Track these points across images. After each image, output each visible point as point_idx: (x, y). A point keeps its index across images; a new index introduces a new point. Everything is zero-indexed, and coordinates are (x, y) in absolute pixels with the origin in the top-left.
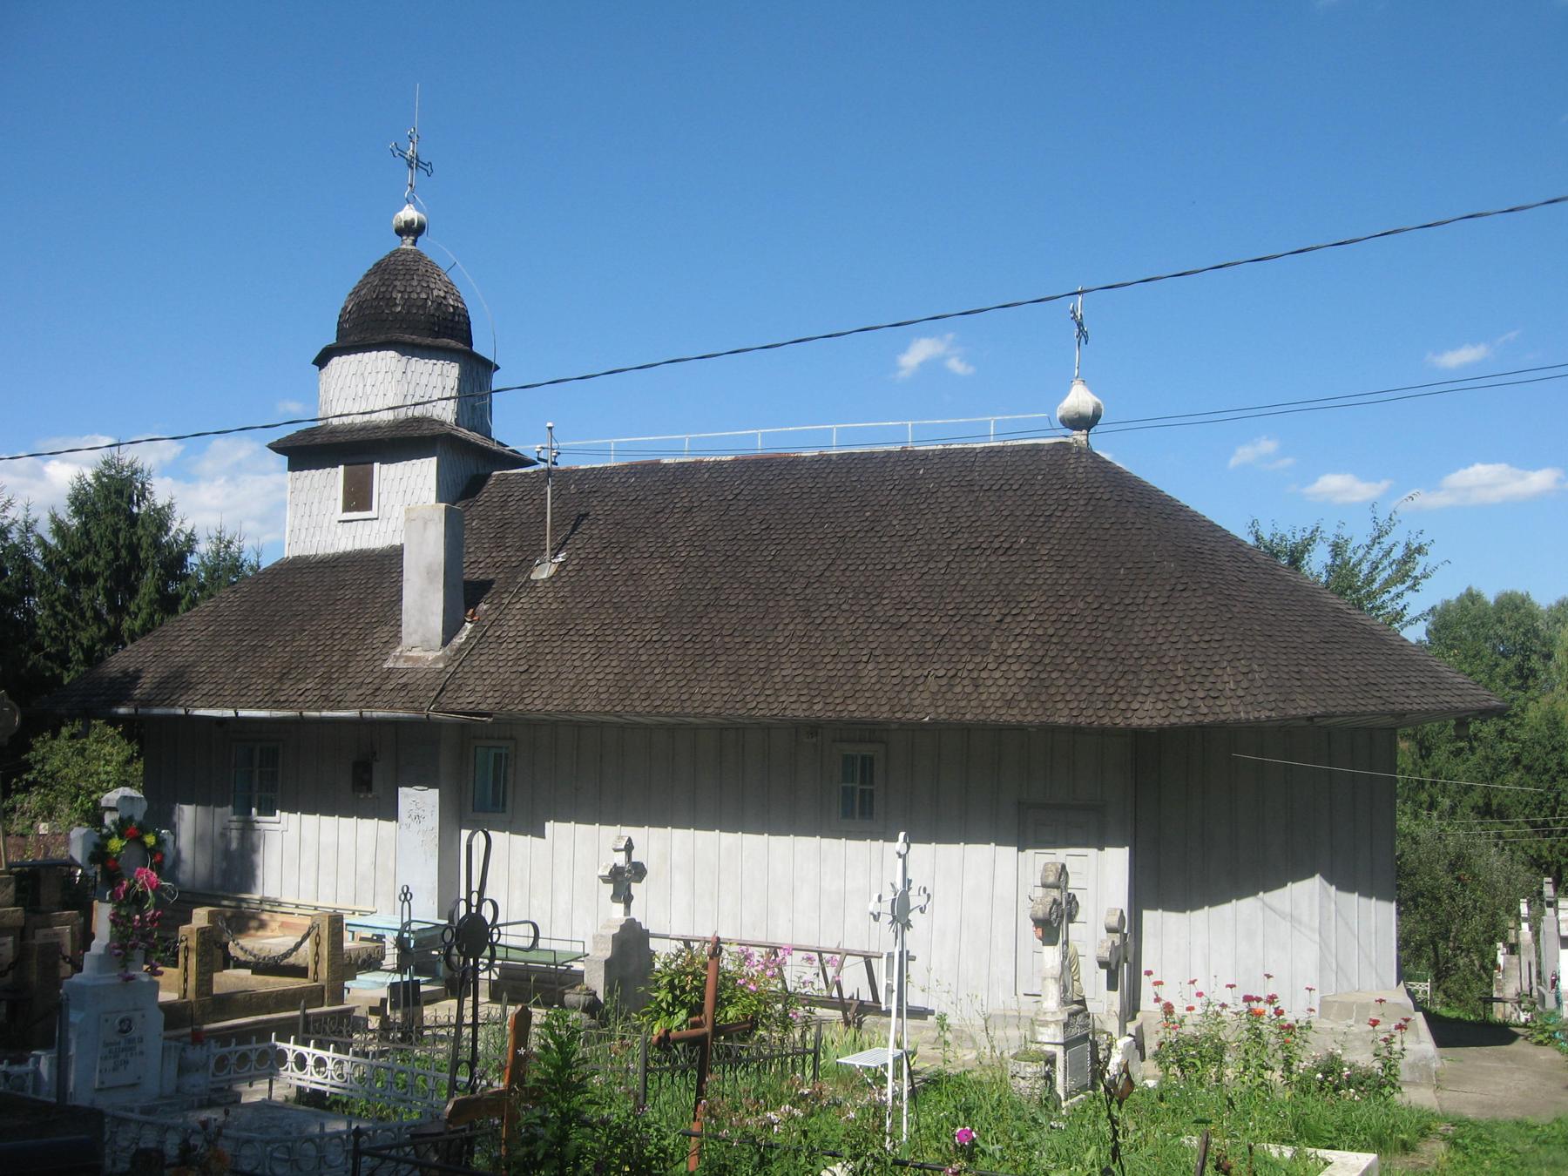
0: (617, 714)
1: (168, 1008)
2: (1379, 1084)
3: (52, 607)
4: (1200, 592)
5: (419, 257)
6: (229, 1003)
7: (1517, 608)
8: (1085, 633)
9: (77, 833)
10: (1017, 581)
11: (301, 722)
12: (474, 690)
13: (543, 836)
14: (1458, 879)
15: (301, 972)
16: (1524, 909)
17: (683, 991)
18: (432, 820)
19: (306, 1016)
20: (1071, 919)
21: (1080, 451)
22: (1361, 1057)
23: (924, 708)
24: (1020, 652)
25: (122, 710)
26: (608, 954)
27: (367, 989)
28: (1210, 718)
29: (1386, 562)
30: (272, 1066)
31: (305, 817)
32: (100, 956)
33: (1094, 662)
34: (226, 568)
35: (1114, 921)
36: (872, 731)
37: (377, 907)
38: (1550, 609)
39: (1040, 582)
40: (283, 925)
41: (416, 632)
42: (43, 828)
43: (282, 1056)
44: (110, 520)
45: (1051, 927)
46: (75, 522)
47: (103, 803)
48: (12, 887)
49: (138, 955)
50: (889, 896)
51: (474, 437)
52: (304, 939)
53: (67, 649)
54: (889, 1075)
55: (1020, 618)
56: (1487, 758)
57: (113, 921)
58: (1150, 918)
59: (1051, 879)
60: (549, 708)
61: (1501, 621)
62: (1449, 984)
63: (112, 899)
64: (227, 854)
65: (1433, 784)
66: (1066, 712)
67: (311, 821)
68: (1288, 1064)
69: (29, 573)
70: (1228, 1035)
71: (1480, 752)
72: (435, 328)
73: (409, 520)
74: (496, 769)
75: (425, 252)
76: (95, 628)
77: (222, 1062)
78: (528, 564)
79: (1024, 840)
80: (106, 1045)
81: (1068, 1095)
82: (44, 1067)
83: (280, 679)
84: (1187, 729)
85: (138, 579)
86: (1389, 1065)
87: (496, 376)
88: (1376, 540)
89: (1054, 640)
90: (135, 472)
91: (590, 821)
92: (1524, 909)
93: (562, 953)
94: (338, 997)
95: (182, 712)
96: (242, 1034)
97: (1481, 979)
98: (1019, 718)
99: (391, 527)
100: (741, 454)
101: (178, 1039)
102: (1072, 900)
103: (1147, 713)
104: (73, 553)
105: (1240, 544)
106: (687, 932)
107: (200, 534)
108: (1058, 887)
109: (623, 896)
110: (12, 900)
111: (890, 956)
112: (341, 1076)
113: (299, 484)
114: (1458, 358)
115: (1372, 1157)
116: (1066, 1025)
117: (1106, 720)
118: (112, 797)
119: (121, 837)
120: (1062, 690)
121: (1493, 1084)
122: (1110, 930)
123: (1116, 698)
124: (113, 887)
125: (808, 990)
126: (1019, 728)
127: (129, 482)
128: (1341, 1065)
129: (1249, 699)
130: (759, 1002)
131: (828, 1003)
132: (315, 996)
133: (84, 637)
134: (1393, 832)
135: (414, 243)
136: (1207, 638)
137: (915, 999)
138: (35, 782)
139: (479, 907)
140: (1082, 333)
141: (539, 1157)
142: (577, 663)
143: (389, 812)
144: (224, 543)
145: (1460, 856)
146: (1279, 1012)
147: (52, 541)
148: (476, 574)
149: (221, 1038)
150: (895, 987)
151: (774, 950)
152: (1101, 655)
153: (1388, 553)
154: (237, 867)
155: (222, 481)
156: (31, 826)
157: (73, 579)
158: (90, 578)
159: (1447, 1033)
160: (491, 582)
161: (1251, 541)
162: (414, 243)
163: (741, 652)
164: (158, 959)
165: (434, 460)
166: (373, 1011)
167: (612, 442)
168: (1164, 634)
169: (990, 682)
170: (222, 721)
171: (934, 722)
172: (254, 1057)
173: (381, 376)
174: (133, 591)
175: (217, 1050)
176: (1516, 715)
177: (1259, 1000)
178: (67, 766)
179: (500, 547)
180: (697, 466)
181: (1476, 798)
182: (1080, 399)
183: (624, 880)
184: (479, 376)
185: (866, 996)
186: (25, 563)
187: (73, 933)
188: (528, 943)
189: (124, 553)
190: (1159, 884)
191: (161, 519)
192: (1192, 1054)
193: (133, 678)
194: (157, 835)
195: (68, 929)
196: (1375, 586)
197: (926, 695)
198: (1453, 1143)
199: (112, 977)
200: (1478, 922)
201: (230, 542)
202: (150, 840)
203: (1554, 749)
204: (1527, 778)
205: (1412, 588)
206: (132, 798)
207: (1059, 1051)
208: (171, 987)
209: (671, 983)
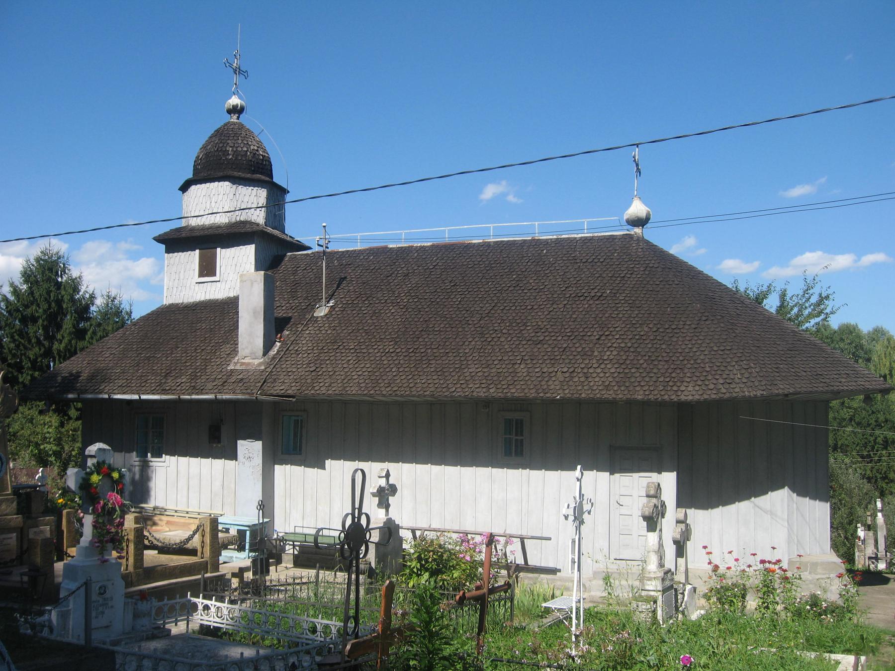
0: (371, 396)
4: (716, 322)
5: (241, 126)
6: (152, 573)
7: (851, 333)
8: (650, 346)
10: (607, 315)
11: (180, 401)
13: (324, 469)
15: (193, 552)
17: (427, 562)
18: (258, 460)
20: (663, 517)
23: (557, 391)
24: (611, 357)
28: (727, 395)
31: (180, 458)
34: (115, 316)
38: (869, 333)
39: (621, 316)
40: (168, 523)
41: (247, 348)
44: (46, 285)
46: (25, 287)
48: (15, 503)
50: (572, 505)
51: (276, 232)
53: (21, 361)
54: (574, 616)
55: (610, 337)
59: (652, 492)
60: (330, 392)
61: (842, 340)
66: (641, 392)
67: (184, 461)
72: (253, 169)
73: (241, 281)
74: (295, 429)
75: (248, 125)
76: (37, 349)
77: (159, 611)
83: (166, 376)
85: (62, 319)
89: (632, 350)
90: (59, 258)
94: (216, 566)
95: (106, 396)
96: (160, 593)
99: (227, 287)
103: (690, 393)
104: (23, 305)
107: (98, 294)
108: (656, 497)
110: (15, 511)
112: (232, 619)
113: (172, 261)
114: (798, 191)
116: (663, 580)
117: (666, 397)
119: (98, 474)
120: (638, 379)
123: (671, 384)
126: (613, 403)
127: (56, 263)
129: (749, 384)
132: (201, 567)
133: (31, 354)
135: (238, 118)
136: (722, 348)
140: (638, 170)
142: (345, 366)
143: (232, 455)
147: (12, 298)
148: (280, 313)
150: (576, 560)
152: (660, 358)
153: (808, 300)
154: (140, 490)
155: (93, 265)
157: (24, 320)
158: (34, 320)
160: (290, 318)
162: (238, 118)
163: (444, 358)
165: (253, 246)
171: (562, 399)
172: (178, 607)
173: (221, 197)
174: (59, 327)
175: (156, 603)
178: (22, 429)
180: (410, 249)
182: (638, 208)
184: (277, 195)
185: (520, 561)
187: (51, 530)
189: (53, 304)
190: (689, 496)
191: (75, 285)
192: (727, 594)
195: (48, 528)
197: (557, 383)
199: (95, 560)
201: (115, 298)
202: (116, 475)
203: (873, 412)
206: (104, 450)
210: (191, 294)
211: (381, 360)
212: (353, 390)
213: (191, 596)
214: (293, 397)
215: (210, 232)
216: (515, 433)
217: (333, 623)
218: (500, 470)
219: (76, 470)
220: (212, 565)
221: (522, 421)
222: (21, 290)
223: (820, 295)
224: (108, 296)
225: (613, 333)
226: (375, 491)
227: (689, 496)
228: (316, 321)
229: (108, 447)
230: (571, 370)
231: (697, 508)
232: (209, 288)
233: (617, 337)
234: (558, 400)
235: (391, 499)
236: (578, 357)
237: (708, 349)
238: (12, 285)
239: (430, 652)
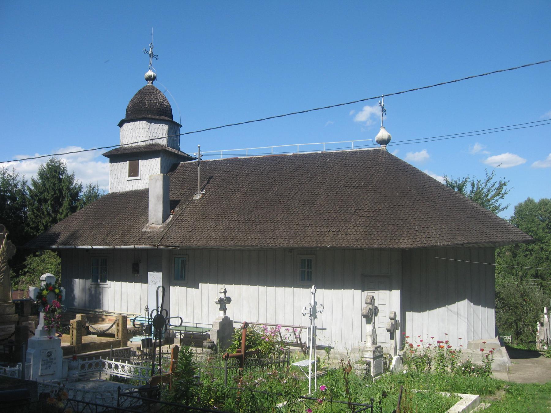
1: (64, 348)
2: (484, 371)
3: (33, 211)
4: (424, 201)
5: (154, 88)
7: (547, 204)
8: (384, 216)
10: (361, 198)
11: (114, 249)
12: (173, 238)
13: (198, 288)
14: (524, 300)
15: (112, 335)
16: (545, 310)
20: (376, 315)
21: (383, 152)
24: (361, 223)
25: (54, 247)
26: (218, 329)
27: (136, 341)
28: (427, 245)
29: (493, 189)
32: (41, 331)
33: (387, 226)
34: (93, 196)
35: (392, 316)
36: (310, 251)
40: (109, 320)
43: (104, 364)
44: (53, 180)
46: (40, 181)
48: (14, 307)
50: (309, 308)
51: (174, 150)
53: (38, 226)
56: (536, 257)
57: (45, 319)
59: (369, 301)
60: (199, 244)
62: (521, 337)
64: (90, 295)
68: (453, 364)
69: (25, 199)
71: (534, 255)
72: (160, 113)
73: (150, 180)
74: (182, 265)
76: (48, 218)
77: (83, 367)
78: (192, 194)
80: (43, 360)
84: (419, 248)
85: (62, 201)
86: (488, 364)
87: (181, 129)
89: (373, 218)
91: (214, 283)
92: (545, 310)
93: (205, 328)
95: (74, 247)
96: (90, 357)
98: (361, 245)
99: (145, 182)
101: (68, 359)
102: (376, 309)
103: (405, 243)
107: (84, 185)
111: (310, 328)
113: (113, 168)
116: (374, 352)
117: (391, 246)
119: (47, 290)
121: (529, 371)
123: (395, 238)
126: (361, 249)
128: (471, 364)
129: (441, 238)
132: (117, 344)
135: (152, 83)
136: (427, 217)
137: (318, 343)
138: (27, 272)
143: (145, 281)
144: (92, 188)
146: (449, 347)
147: (32, 188)
148: (173, 198)
149: (85, 359)
150: (311, 339)
152: (389, 223)
153: (494, 185)
157: (40, 201)
158: (46, 201)
159: (513, 353)
160: (180, 201)
162: (152, 83)
169: (351, 233)
170: (87, 250)
171: (331, 247)
172: (94, 364)
174: (61, 205)
175: (81, 362)
176: (547, 242)
177: (442, 342)
178: (38, 266)
179: (183, 188)
180: (251, 159)
181: (532, 271)
182: (383, 134)
183: (223, 303)
184: (175, 129)
186: (23, 195)
189: (57, 192)
191: (70, 180)
193: (58, 235)
194: (59, 289)
196: (489, 197)
198: (508, 391)
200: (531, 315)
201: (94, 187)
202: (57, 291)
205: (502, 197)
206: (51, 277)
207: (372, 361)
208: (66, 341)
211: (229, 225)
213: (102, 358)
215: (135, 150)
218: (299, 289)
220: (123, 342)
222: (38, 183)
227: (408, 305)
235: (227, 305)
238: (33, 180)
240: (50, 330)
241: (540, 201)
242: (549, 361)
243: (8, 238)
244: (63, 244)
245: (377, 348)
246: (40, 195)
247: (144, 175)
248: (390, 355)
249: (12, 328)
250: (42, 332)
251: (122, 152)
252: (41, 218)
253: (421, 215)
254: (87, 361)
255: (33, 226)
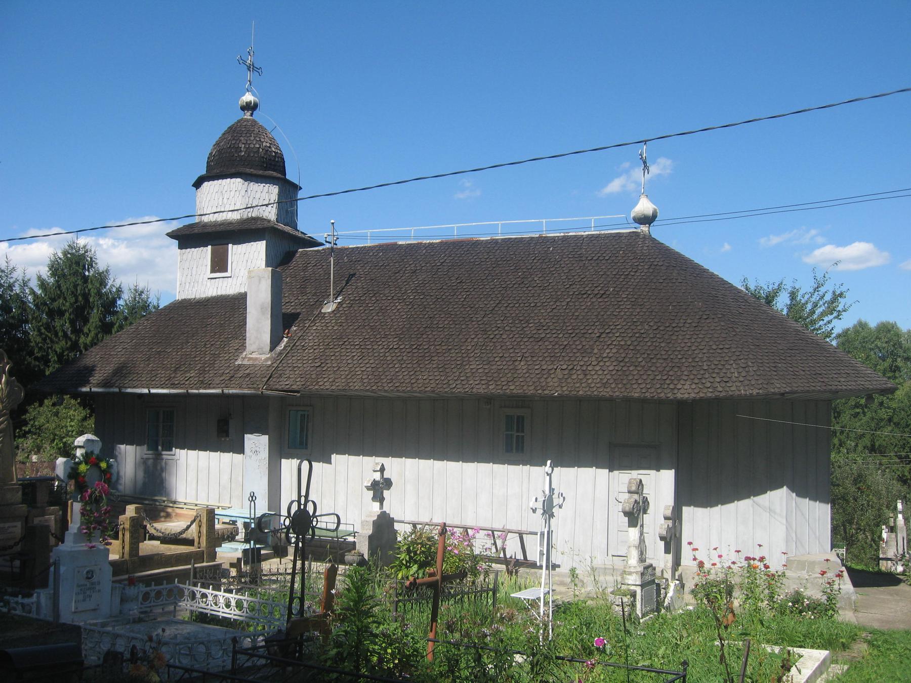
1: (114, 564)
4: (716, 320)
5: (254, 121)
7: (889, 331)
8: (649, 344)
9: (61, 461)
10: (608, 313)
11: (188, 396)
14: (859, 488)
15: (190, 542)
16: (900, 506)
17: (415, 553)
18: (264, 454)
19: (195, 568)
20: (645, 512)
21: (645, 237)
22: (814, 593)
23: (555, 387)
24: (611, 355)
26: (370, 532)
27: (230, 552)
28: (723, 394)
29: (821, 303)
30: (175, 598)
31: (190, 452)
36: (522, 401)
37: (232, 504)
39: (622, 313)
42: (34, 458)
44: (73, 279)
45: (634, 515)
46: (52, 280)
47: (76, 444)
48: (20, 493)
49: (98, 533)
50: (541, 499)
51: (287, 229)
52: (192, 523)
53: (48, 354)
55: (611, 335)
56: (873, 419)
58: (687, 511)
59: (634, 488)
60: (333, 387)
63: (82, 500)
64: (146, 471)
65: (842, 432)
68: (771, 597)
69: (25, 310)
70: (735, 580)
71: (869, 415)
72: (265, 165)
73: (250, 277)
74: (303, 423)
75: (261, 122)
76: (64, 342)
77: (146, 596)
78: (320, 304)
79: (614, 463)
80: (78, 586)
81: (643, 616)
82: (43, 600)
83: (175, 371)
88: (816, 289)
89: (631, 347)
94: (213, 556)
95: (117, 390)
97: (871, 546)
100: (445, 239)
101: (120, 581)
103: (686, 391)
105: (739, 291)
106: (414, 519)
107: (125, 288)
108: (637, 493)
109: (379, 498)
111: (542, 534)
113: (185, 257)
115: (827, 652)
116: (642, 574)
117: (662, 395)
118: (80, 440)
119: (86, 464)
122: (666, 518)
123: (668, 382)
124: (81, 493)
125: (488, 553)
126: (611, 400)
127: (83, 256)
129: (746, 382)
130: (460, 560)
131: (498, 561)
132: (199, 557)
134: (829, 463)
135: (252, 115)
136: (721, 347)
138: (29, 432)
139: (305, 505)
141: (345, 655)
145: (860, 476)
146: (766, 567)
147: (39, 292)
148: (289, 309)
149: (150, 583)
150: (545, 552)
151: (466, 529)
152: (659, 356)
153: (822, 297)
156: (28, 457)
157: (51, 313)
158: (61, 313)
159: (861, 579)
160: (299, 314)
161: (743, 289)
162: (252, 115)
164: (109, 536)
165: (264, 242)
166: (232, 565)
167: (369, 232)
168: (696, 344)
171: (560, 396)
172: (165, 593)
174: (86, 321)
175: (143, 588)
178: (48, 422)
180: (418, 246)
181: (866, 441)
182: (644, 206)
183: (379, 488)
184: (289, 193)
185: (520, 556)
186: (23, 304)
188: (333, 527)
189: (80, 298)
190: (690, 493)
191: (102, 278)
192: (714, 592)
193: (89, 371)
194: (108, 462)
195: (53, 517)
196: (815, 316)
198: (870, 643)
200: (870, 514)
202: (103, 465)
204: (896, 430)
205: (837, 317)
206: (93, 441)
207: (638, 590)
208: (115, 552)
209: (408, 549)
210: (203, 289)
212: (356, 386)
214: (298, 392)
215: (222, 228)
216: (512, 428)
217: (246, 598)
219: (65, 459)
221: (523, 417)
223: (834, 292)
224: (136, 290)
225: (614, 331)
226: (369, 484)
227: (690, 493)
228: (324, 317)
229: (96, 438)
230: (570, 367)
231: (697, 505)
232: (220, 284)
233: (617, 335)
234: (556, 397)
235: (386, 493)
236: (578, 354)
237: (707, 347)
238: (39, 278)
239: (359, 630)
240: (91, 533)
241: (878, 325)
242: (908, 588)
243: (11, 373)
244: (106, 384)
245: (646, 568)
246: (51, 303)
247: (237, 270)
248: (667, 580)
249: (17, 529)
250: (79, 536)
251: (200, 231)
252: (52, 341)
253: (711, 343)
254: (153, 587)
255: (39, 355)
